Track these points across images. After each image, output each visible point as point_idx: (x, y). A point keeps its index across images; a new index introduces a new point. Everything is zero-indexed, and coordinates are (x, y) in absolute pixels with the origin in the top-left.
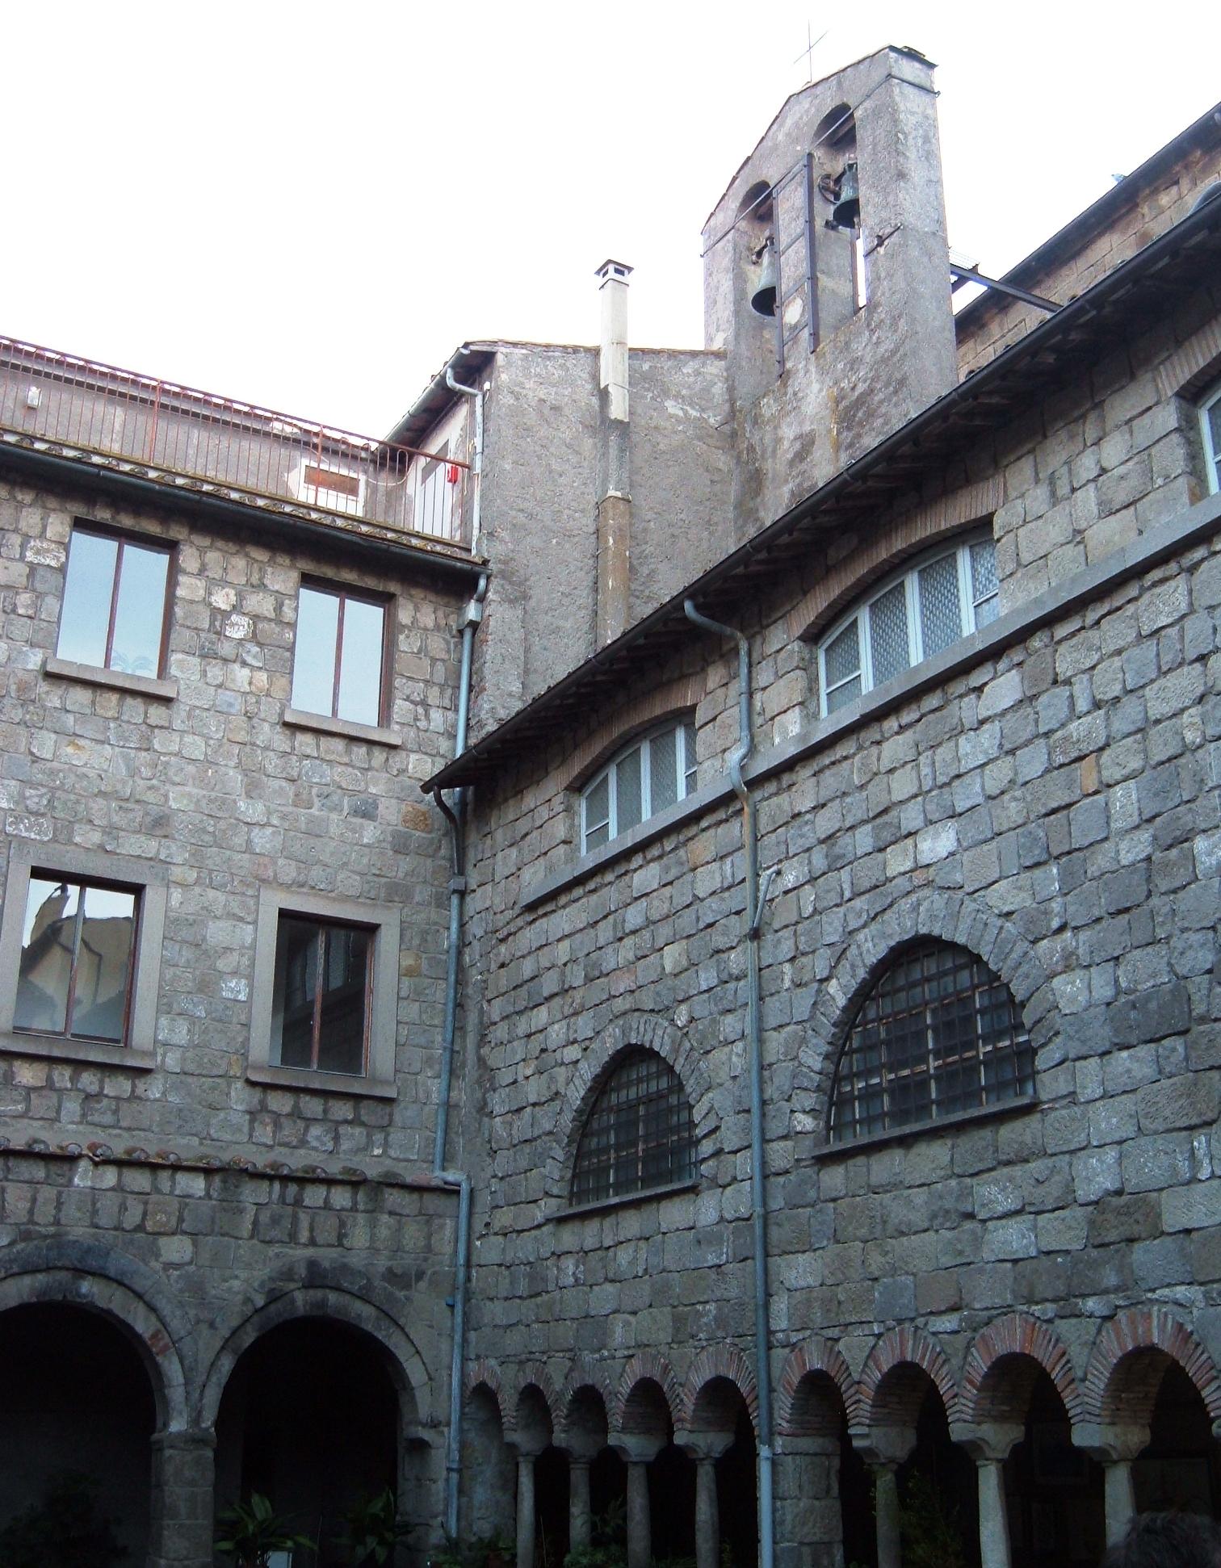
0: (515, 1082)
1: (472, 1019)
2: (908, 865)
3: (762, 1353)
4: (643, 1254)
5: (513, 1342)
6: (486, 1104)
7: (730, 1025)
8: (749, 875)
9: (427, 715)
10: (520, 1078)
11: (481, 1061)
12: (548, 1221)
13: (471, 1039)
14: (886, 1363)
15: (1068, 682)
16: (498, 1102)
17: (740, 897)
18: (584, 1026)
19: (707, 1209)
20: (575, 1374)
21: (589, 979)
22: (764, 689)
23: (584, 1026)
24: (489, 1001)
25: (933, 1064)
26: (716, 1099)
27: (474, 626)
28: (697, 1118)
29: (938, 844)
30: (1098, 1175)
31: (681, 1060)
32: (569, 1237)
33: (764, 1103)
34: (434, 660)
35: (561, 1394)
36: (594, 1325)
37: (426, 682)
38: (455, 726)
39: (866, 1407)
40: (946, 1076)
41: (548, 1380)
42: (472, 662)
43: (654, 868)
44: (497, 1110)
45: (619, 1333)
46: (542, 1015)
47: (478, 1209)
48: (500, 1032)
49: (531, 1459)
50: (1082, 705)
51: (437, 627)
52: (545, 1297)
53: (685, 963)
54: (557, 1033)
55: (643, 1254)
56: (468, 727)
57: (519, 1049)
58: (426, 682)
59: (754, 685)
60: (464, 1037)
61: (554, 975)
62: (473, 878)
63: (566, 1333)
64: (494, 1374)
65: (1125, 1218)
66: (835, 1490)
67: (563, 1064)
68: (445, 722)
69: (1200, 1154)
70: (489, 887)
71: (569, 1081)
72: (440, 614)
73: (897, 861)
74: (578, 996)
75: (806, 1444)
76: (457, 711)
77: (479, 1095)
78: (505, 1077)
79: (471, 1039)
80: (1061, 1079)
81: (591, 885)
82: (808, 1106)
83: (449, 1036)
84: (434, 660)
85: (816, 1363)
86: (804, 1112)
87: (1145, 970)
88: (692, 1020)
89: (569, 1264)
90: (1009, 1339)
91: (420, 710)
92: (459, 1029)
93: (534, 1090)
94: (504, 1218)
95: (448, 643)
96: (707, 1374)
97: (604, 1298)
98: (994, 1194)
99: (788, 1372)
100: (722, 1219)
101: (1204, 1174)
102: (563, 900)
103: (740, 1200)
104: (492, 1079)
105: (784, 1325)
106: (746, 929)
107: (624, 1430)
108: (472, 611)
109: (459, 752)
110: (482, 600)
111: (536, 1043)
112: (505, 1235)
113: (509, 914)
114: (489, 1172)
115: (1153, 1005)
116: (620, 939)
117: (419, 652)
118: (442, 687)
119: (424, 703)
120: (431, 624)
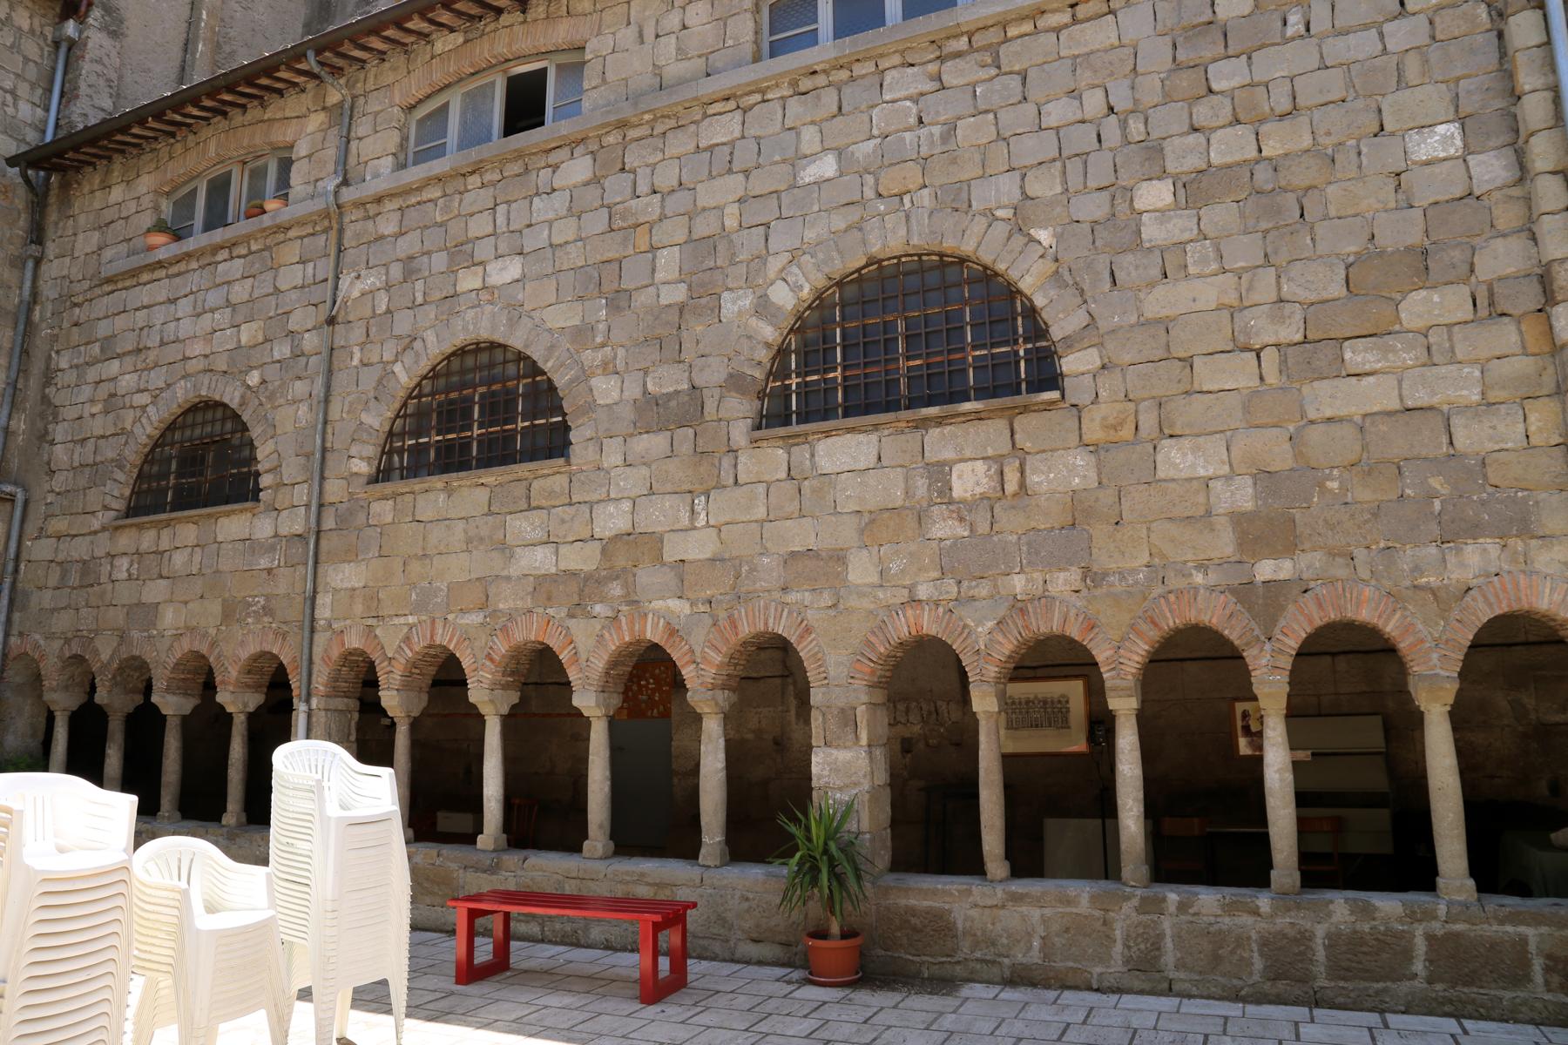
0: (80, 418)
1: (37, 368)
2: (478, 284)
3: (307, 634)
4: (197, 558)
5: (62, 622)
6: (47, 432)
7: (300, 388)
8: (331, 276)
9: (15, 105)
10: (86, 414)
11: (45, 400)
12: (104, 529)
13: (34, 382)
14: (419, 644)
15: (634, 172)
16: (59, 432)
17: (319, 293)
18: (157, 379)
19: (264, 528)
20: (123, 648)
21: (162, 344)
22: (360, 139)
23: (157, 379)
24: (58, 352)
25: (476, 432)
26: (276, 451)
27: (72, 44)
28: (260, 456)
29: (506, 272)
30: (612, 520)
31: (249, 411)
32: (125, 541)
33: (324, 450)
34: (26, 60)
35: (105, 666)
36: (146, 613)
37: (17, 75)
38: (46, 122)
39: (397, 676)
40: (487, 443)
41: (96, 652)
42: (65, 73)
43: (239, 262)
44: (58, 438)
45: (169, 618)
46: (114, 367)
47: (31, 516)
48: (70, 377)
49: (68, 713)
50: (643, 188)
51: (32, 31)
52: (96, 588)
53: (261, 339)
54: (128, 382)
55: (197, 558)
56: (57, 126)
57: (87, 391)
58: (17, 75)
59: (353, 134)
60: (27, 380)
61: (132, 336)
62: (51, 249)
63: (117, 617)
64: (37, 646)
65: (640, 544)
66: (353, 738)
67: (132, 407)
68: (33, 115)
69: (698, 508)
70: (67, 260)
71: (137, 420)
72: (36, 22)
73: (468, 281)
74: (152, 356)
75: (340, 703)
76: (47, 110)
77: (40, 425)
78: (70, 413)
79: (34, 382)
80: (591, 449)
81: (174, 270)
82: (365, 454)
83: (13, 376)
84: (26, 60)
85: (354, 641)
86: (361, 458)
87: (668, 381)
88: (264, 382)
89: (124, 563)
90: (527, 632)
91: (9, 98)
92: (23, 371)
93: (98, 426)
94: (59, 525)
95: (42, 49)
96: (253, 648)
97: (155, 591)
98: (524, 526)
99: (327, 652)
100: (276, 535)
101: (701, 521)
102: (145, 277)
103: (295, 523)
104: (55, 415)
105: (328, 614)
106: (322, 318)
107: (168, 690)
108: (70, 28)
109: (49, 138)
110: (82, 21)
111: (104, 390)
112: (59, 538)
113: (86, 284)
114: (47, 487)
115: (673, 404)
116: (198, 315)
117: (12, 46)
118: (33, 86)
119: (13, 92)
120: (26, 25)
